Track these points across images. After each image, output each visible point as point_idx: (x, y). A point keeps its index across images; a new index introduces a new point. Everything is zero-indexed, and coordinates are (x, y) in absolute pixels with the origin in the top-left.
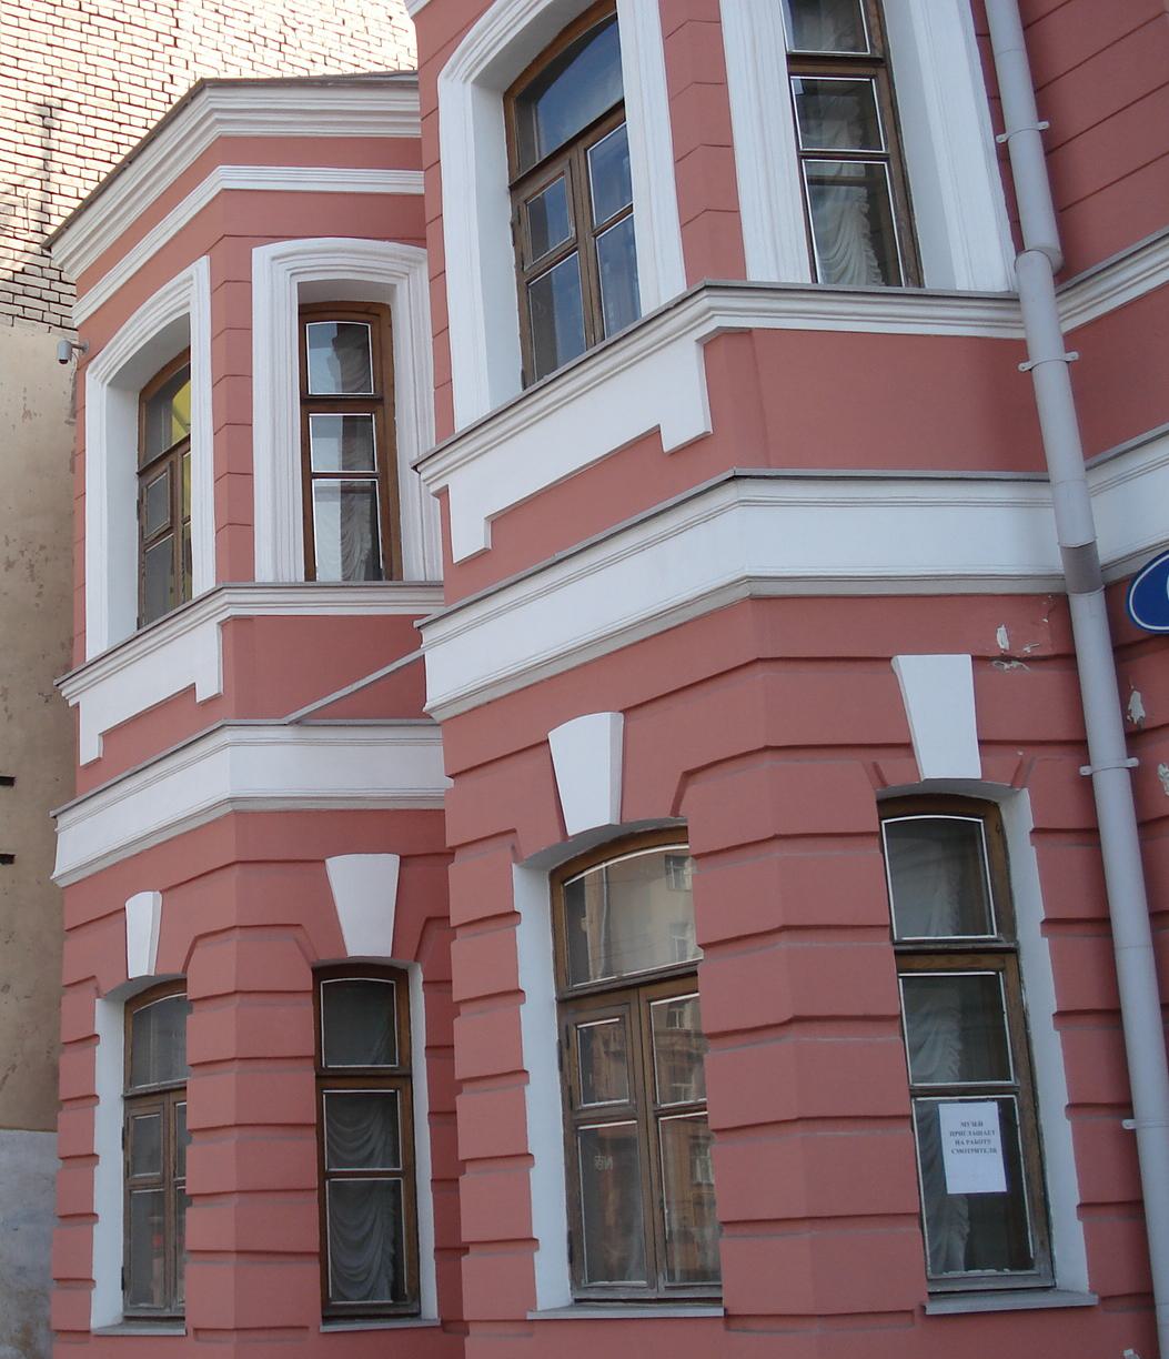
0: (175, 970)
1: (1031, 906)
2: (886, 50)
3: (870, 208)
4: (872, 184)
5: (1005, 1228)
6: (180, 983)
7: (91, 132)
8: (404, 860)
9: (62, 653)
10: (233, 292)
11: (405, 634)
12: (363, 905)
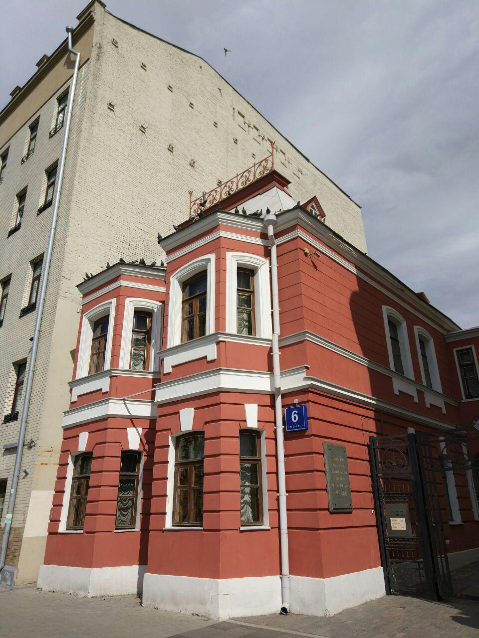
1: (264, 452)
3: (249, 325)
4: (249, 321)
10: (120, 307)
11: (202, 461)
12: (134, 439)
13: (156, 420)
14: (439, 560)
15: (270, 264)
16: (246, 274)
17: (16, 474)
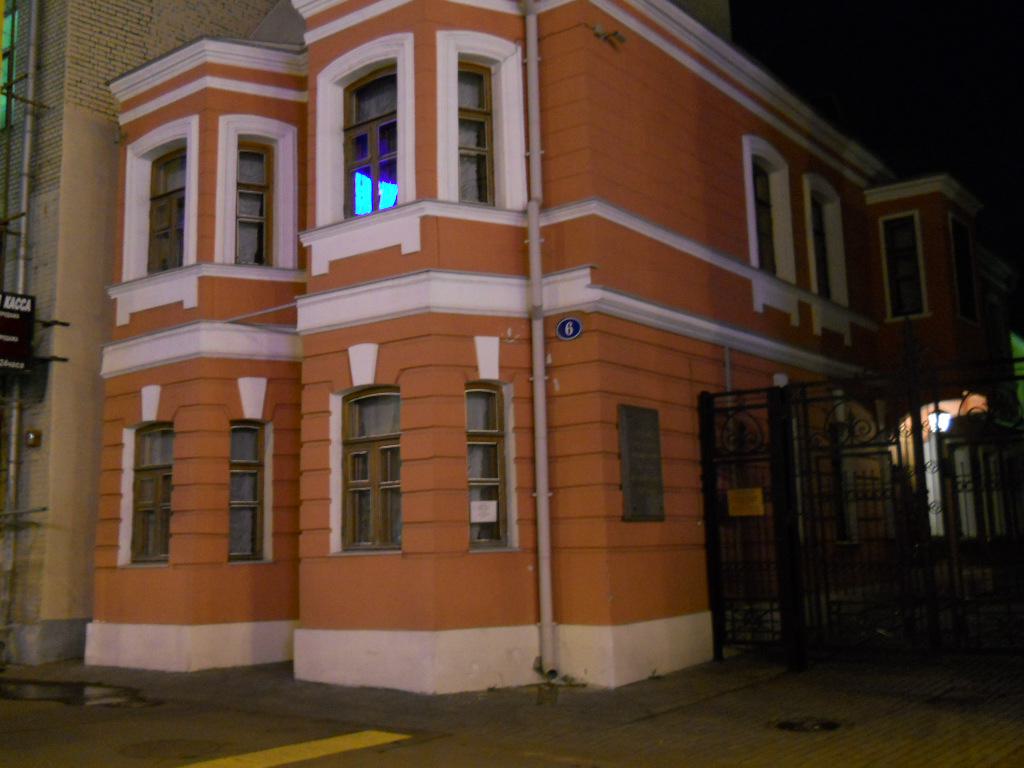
0: (168, 419)
1: (510, 422)
2: (491, 110)
5: (493, 532)
6: (171, 424)
7: (114, 13)
8: (270, 381)
9: (111, 270)
13: (300, 364)
14: (806, 604)
15: (525, 54)
16: (475, 75)
17: (984, 495)
